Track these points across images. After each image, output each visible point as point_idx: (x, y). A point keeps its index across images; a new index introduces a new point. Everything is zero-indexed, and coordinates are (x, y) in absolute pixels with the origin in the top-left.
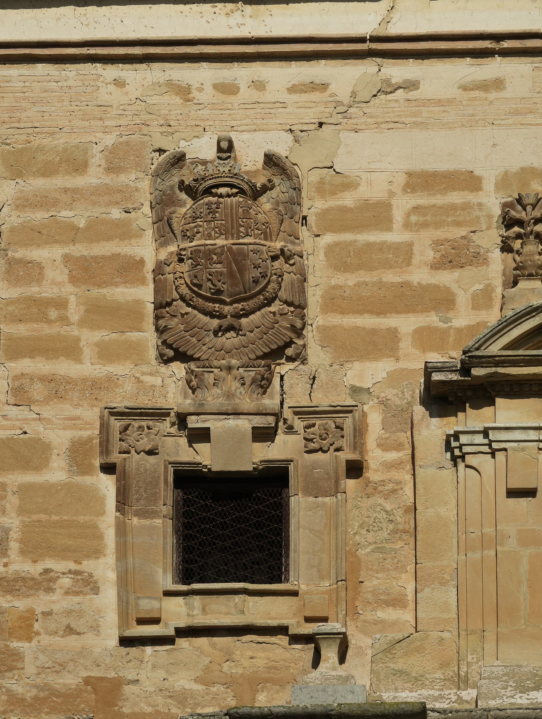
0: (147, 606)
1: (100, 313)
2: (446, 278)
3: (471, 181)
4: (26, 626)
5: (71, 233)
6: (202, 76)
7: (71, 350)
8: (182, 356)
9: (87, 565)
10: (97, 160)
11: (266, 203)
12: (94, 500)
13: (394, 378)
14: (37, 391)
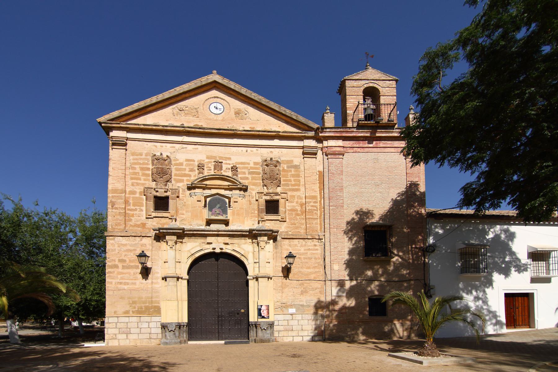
0: (150, 213)
1: (144, 175)
2: (190, 173)
3: (194, 161)
4: (133, 216)
5: (140, 164)
6: (158, 145)
7: (140, 179)
8: (155, 181)
9: (141, 208)
10: (144, 154)
11: (167, 162)
12: (143, 199)
13: (183, 186)
14: (135, 184)
